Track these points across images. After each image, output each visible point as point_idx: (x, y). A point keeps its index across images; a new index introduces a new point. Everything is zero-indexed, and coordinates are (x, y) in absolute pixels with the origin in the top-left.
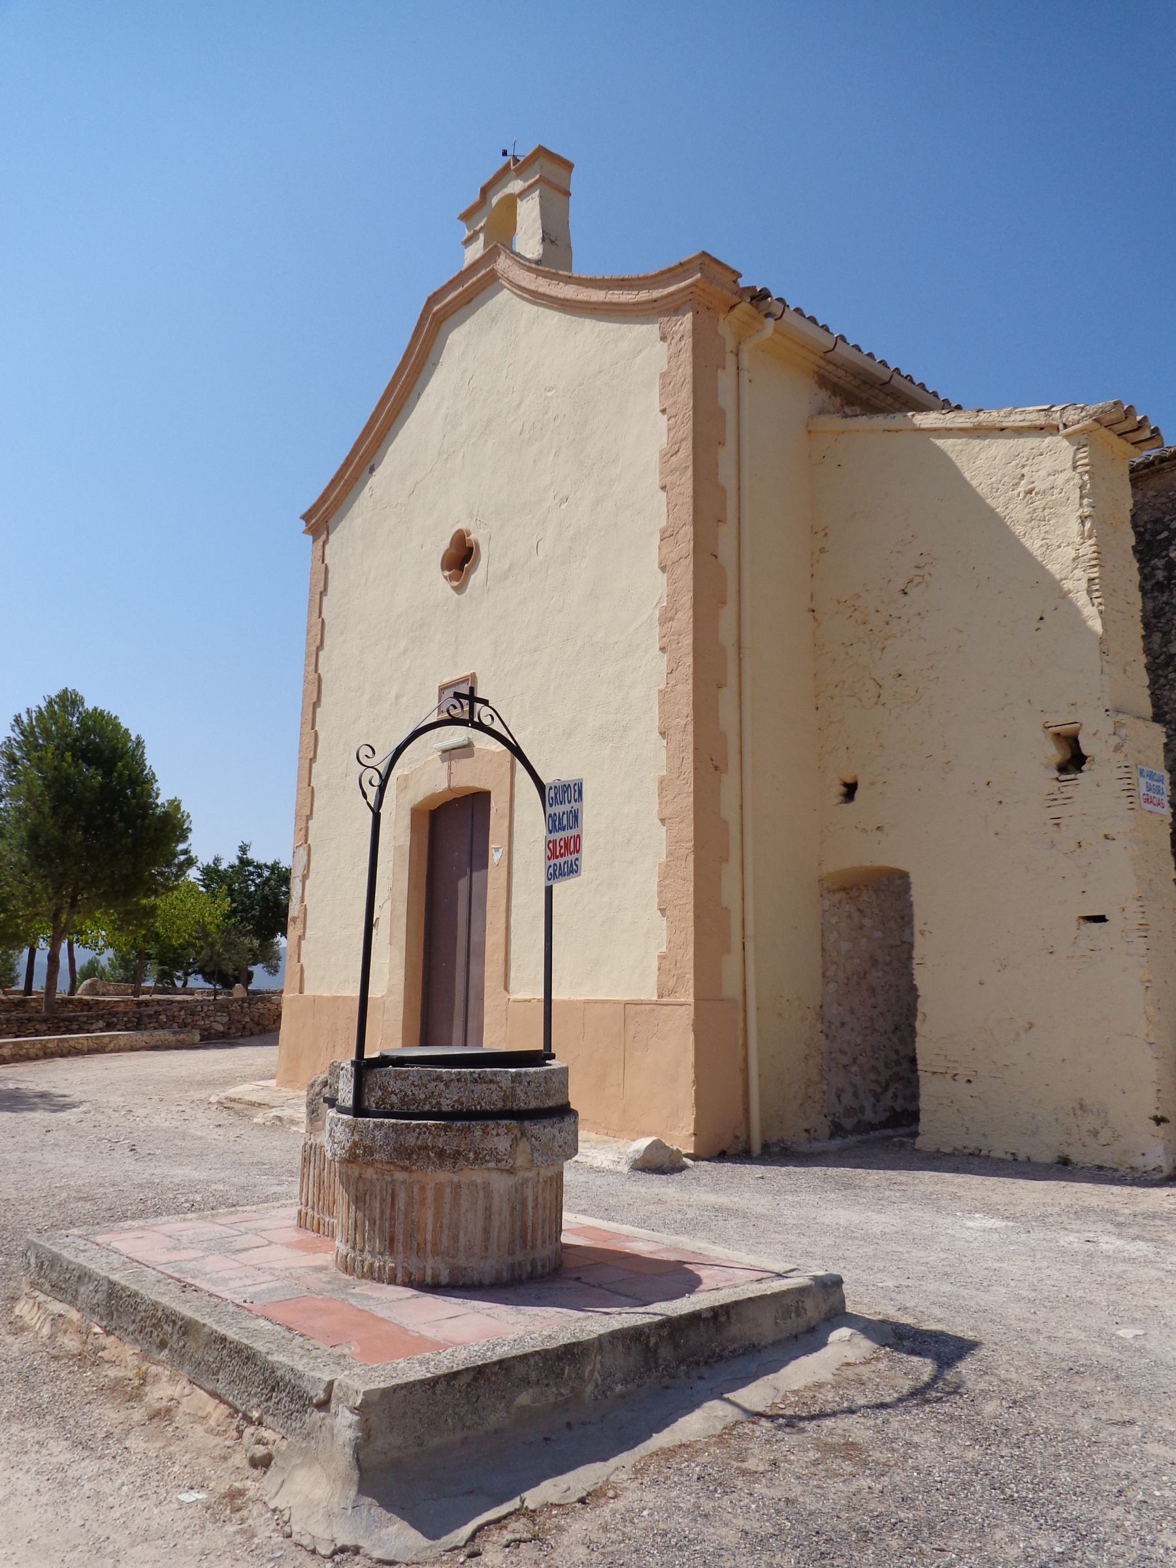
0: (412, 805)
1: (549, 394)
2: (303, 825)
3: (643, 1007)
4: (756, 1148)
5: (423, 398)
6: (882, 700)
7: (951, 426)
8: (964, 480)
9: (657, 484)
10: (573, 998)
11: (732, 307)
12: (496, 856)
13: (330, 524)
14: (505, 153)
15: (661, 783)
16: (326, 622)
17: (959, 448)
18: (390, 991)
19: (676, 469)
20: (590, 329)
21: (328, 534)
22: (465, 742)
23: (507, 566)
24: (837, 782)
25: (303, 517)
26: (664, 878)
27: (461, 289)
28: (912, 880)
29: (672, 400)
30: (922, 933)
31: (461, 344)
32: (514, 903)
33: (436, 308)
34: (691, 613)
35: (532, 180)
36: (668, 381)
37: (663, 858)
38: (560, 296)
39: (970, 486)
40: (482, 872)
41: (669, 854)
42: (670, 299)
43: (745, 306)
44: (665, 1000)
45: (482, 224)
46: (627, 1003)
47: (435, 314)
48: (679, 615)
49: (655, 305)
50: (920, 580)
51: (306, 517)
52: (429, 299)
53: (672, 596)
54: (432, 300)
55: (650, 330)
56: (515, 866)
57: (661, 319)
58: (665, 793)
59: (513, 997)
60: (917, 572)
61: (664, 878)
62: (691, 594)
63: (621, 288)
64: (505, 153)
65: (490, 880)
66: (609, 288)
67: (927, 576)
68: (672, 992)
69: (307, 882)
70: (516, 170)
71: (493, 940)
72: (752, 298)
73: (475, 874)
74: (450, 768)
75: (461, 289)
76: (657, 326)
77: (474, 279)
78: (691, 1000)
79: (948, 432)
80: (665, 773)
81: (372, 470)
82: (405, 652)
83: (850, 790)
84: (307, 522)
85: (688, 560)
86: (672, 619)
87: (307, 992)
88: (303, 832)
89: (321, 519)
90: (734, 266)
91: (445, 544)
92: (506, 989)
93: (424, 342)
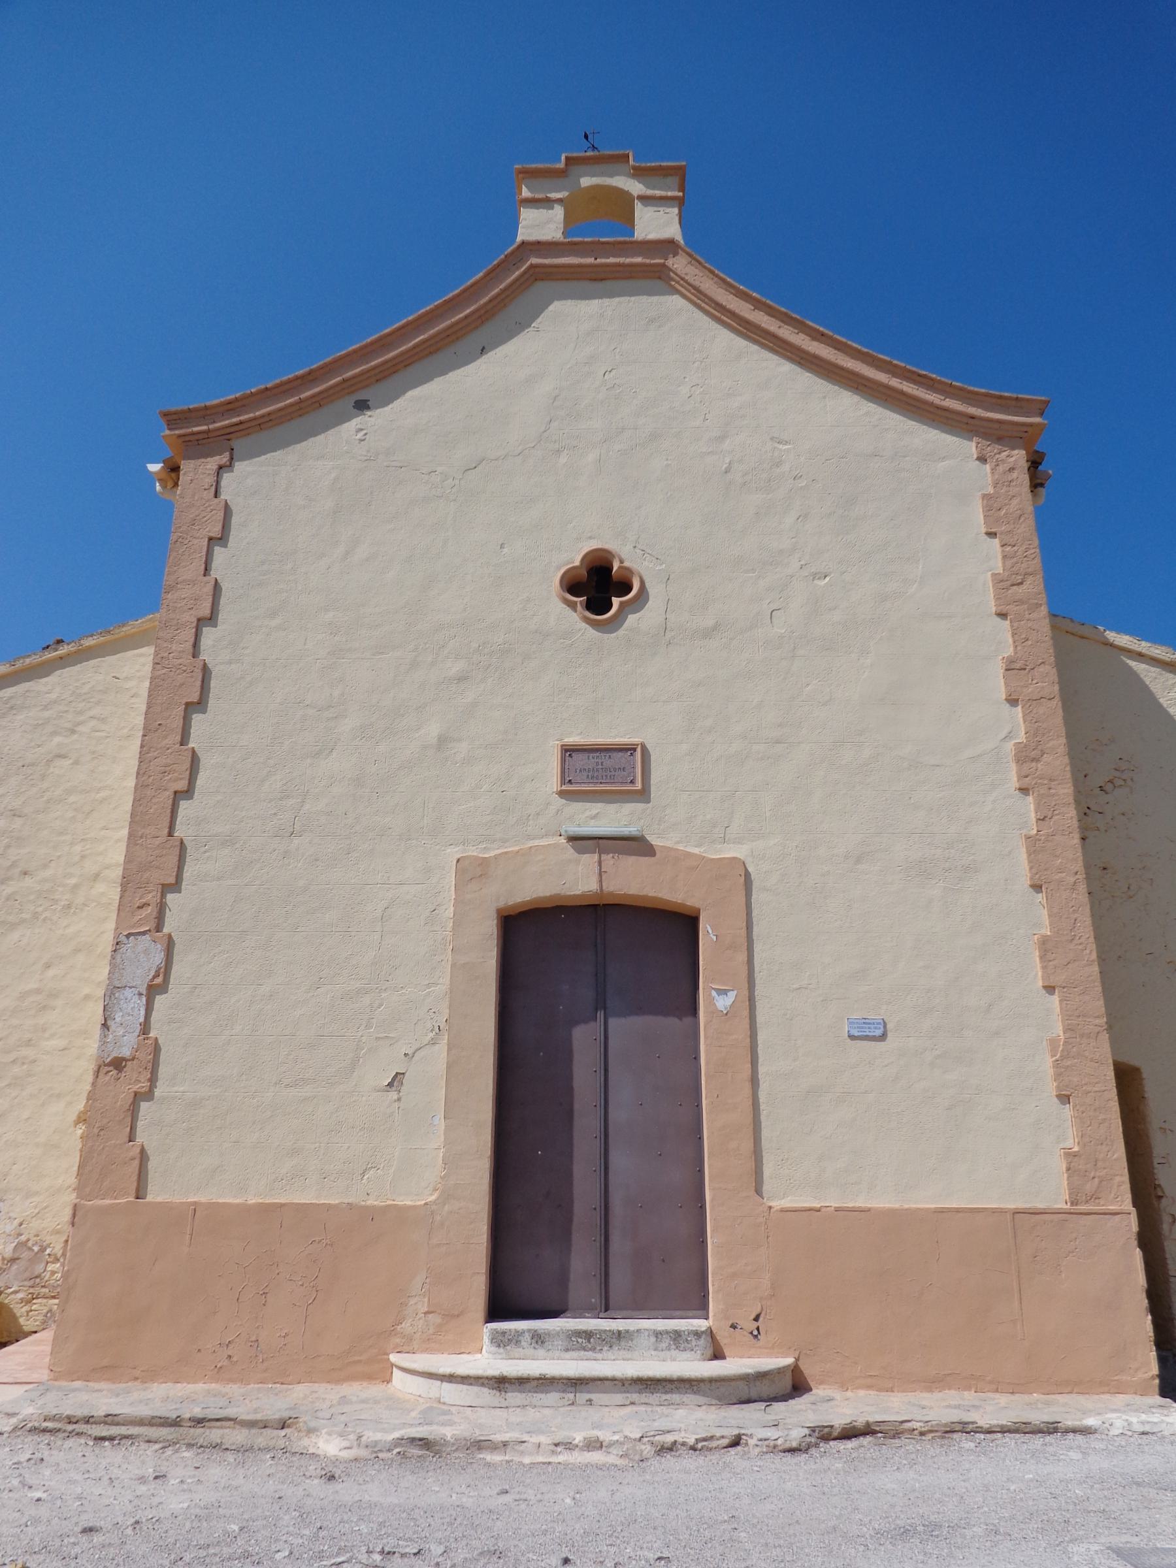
3: (1046, 1217)
8: (1161, 706)
10: (906, 1206)
16: (225, 586)
18: (447, 1196)
20: (846, 401)
27: (590, 260)
32: (762, 1070)
33: (535, 260)
37: (1059, 1030)
42: (996, 426)
44: (1083, 1208)
46: (1016, 1212)
47: (532, 266)
49: (971, 421)
53: (1036, 732)
55: (971, 447)
59: (777, 1204)
60: (1117, 774)
63: (914, 382)
67: (1129, 782)
68: (1094, 1197)
73: (613, 1022)
79: (1140, 656)
81: (362, 406)
82: (461, 679)
91: (575, 559)
92: (759, 1191)
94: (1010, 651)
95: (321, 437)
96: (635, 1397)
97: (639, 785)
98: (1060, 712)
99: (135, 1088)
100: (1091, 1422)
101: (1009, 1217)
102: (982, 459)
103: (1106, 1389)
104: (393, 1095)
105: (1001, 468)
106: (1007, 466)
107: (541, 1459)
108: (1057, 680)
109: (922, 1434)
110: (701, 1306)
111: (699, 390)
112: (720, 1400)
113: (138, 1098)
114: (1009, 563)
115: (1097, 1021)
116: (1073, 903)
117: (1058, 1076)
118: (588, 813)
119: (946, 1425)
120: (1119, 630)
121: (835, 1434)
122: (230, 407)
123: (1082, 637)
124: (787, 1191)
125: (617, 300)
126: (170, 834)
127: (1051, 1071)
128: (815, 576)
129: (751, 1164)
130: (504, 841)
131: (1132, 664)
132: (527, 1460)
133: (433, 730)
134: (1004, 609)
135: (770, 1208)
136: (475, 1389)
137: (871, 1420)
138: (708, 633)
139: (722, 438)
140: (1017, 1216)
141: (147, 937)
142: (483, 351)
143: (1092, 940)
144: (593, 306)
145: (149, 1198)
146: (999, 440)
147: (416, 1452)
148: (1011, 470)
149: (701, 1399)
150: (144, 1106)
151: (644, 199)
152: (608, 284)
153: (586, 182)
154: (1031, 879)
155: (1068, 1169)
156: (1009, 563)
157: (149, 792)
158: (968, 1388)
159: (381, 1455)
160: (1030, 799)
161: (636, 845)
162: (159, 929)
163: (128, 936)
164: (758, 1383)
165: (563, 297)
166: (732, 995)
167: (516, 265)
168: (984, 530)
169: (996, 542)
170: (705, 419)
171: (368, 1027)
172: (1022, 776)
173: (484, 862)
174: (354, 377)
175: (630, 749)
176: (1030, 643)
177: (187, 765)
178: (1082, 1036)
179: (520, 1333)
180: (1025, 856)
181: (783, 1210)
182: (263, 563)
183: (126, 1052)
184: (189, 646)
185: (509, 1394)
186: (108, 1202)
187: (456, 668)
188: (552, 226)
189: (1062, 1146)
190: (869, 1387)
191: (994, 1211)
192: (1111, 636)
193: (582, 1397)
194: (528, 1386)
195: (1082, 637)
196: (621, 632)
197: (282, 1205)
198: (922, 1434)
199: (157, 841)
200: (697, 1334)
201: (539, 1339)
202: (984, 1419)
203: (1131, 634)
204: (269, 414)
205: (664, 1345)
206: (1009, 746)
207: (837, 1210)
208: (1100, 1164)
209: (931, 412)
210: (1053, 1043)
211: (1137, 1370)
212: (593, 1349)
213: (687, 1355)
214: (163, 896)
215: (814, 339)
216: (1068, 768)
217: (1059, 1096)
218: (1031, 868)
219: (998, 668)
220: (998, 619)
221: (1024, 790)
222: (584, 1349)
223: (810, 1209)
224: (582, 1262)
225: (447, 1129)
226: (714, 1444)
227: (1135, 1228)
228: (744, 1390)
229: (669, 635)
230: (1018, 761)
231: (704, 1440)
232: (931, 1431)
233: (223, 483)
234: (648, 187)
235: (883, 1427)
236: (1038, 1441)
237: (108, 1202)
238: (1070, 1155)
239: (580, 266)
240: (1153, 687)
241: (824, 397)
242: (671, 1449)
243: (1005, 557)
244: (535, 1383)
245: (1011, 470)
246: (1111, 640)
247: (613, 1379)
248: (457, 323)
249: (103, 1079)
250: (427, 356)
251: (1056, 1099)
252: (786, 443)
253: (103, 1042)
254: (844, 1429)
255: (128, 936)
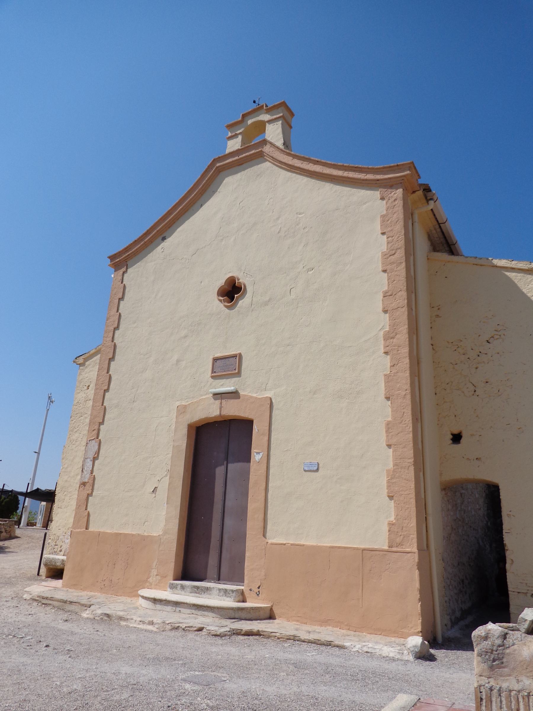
0: (189, 422)
1: (300, 216)
2: (96, 427)
3: (377, 552)
4: (440, 639)
5: (204, 207)
6: (477, 393)
7: (515, 267)
8: (523, 293)
9: (380, 269)
10: (319, 545)
11: (414, 192)
12: (257, 456)
13: (129, 263)
14: (254, 102)
15: (388, 425)
16: (122, 315)
17: (520, 278)
18: (165, 532)
19: (393, 263)
20: (328, 188)
21: (127, 268)
22: (234, 391)
23: (268, 299)
24: (449, 433)
25: (109, 257)
26: (392, 479)
27: (237, 158)
28: (500, 488)
29: (389, 229)
30: (508, 515)
31: (232, 186)
32: (270, 485)
33: (218, 165)
34: (407, 336)
35: (278, 116)
36: (387, 219)
37: (391, 466)
38: (310, 169)
39: (527, 296)
40: (248, 464)
41: (395, 465)
43: (420, 193)
44: (394, 549)
45: (240, 131)
46: (364, 550)
47: (217, 167)
48: (398, 336)
49: (378, 182)
50: (498, 337)
51: (112, 258)
52: (214, 159)
53: (394, 326)
54: (215, 161)
55: (377, 194)
56: (272, 464)
57: (381, 189)
58: (390, 431)
59: (270, 541)
61: (392, 479)
62: (406, 326)
63: (354, 171)
64: (254, 102)
65: (252, 470)
66: (346, 170)
68: (400, 544)
69: (96, 462)
70: (266, 110)
71: (254, 505)
72: (424, 190)
73: (229, 465)
74: (221, 403)
75: (237, 158)
76: (379, 192)
77: (247, 154)
78: (415, 550)
79: (513, 269)
80: (390, 419)
81: (164, 239)
82: (185, 337)
83: (457, 438)
84: (111, 261)
85: (404, 309)
86: (393, 338)
87: (91, 529)
88: (96, 432)
89: (122, 260)
90: (420, 173)
92: (264, 536)
93: (208, 179)
94: (386, 288)
95: (151, 254)
96: (193, 611)
97: (237, 371)
98: (406, 313)
99: (88, 492)
100: (347, 644)
101: (360, 551)
102: (382, 199)
103: (396, 635)
104: (154, 495)
105: (390, 201)
106: (393, 199)
107: (135, 626)
108: (406, 298)
109: (278, 638)
110: (240, 580)
111: (272, 200)
112: (221, 616)
113: (89, 495)
114: (390, 245)
115: (409, 461)
116: (403, 405)
117: (389, 487)
118: (220, 384)
119: (288, 636)
120: (501, 258)
121: (243, 633)
122: (126, 250)
123: (481, 265)
124: (275, 537)
125: (246, 171)
126: (102, 405)
127: (386, 485)
128: (308, 270)
129: (262, 524)
130: (193, 398)
131: (508, 274)
132: (131, 625)
133: (175, 358)
134: (385, 268)
135: (267, 542)
136: (148, 602)
137: (260, 630)
138: (266, 303)
139: (278, 218)
140: (364, 551)
141: (94, 441)
142: (201, 206)
143: (411, 421)
144: (239, 176)
145: (90, 530)
146: (391, 187)
147: (106, 618)
148: (395, 200)
149: (214, 615)
150: (90, 498)
151: (270, 122)
152: (244, 165)
153: (250, 122)
154: (385, 394)
155: (389, 531)
156: (390, 245)
157: (98, 391)
158: (337, 627)
159: (96, 618)
160: (389, 357)
161: (234, 395)
162: (97, 438)
163: (89, 441)
164: (240, 612)
165: (227, 176)
166: (261, 454)
167: (212, 169)
168: (380, 232)
169: (385, 237)
170: (273, 212)
171: (149, 470)
172: (386, 347)
173: (185, 407)
174: (160, 229)
175: (234, 356)
176: (395, 282)
177: (108, 380)
178: (402, 468)
179: (177, 585)
180: (383, 384)
181: (272, 544)
182: (133, 304)
183: (86, 480)
184: (111, 338)
185: (157, 605)
186: (79, 530)
187: (183, 333)
188: (237, 145)
189: (389, 520)
190: (298, 621)
191: (354, 549)
192: (496, 262)
193: (178, 609)
194: (163, 603)
195: (481, 265)
196: (236, 309)
197: (121, 534)
198: (278, 638)
199: (99, 407)
200: (233, 591)
201: (183, 587)
202: (304, 636)
203: (504, 258)
204: (137, 249)
205: (221, 594)
206: (382, 333)
207: (292, 545)
208: (404, 529)
209: (361, 183)
210: (388, 471)
211: (411, 628)
212: (199, 593)
213: (228, 599)
214: (99, 426)
215: (315, 164)
216: (407, 339)
217: (389, 496)
218: (386, 390)
219: (380, 296)
220: (383, 273)
221: (386, 353)
222: (196, 593)
223: (282, 544)
224: (213, 561)
225: (167, 508)
226: (192, 629)
227: (417, 560)
228: (232, 614)
229: (253, 306)
230: (384, 340)
231: (189, 627)
232: (282, 638)
233: (125, 278)
234: (272, 115)
235: (264, 633)
236: (323, 648)
237: (79, 530)
238: (391, 524)
239: (233, 161)
240: (519, 285)
241: (319, 189)
242: (177, 629)
243: (388, 243)
244: (164, 602)
245: (395, 200)
246: (496, 263)
247: (187, 604)
248: (192, 198)
249: (81, 489)
250: (184, 214)
251: (387, 498)
252: (302, 213)
253: (82, 477)
254: (246, 632)
255: (89, 441)
